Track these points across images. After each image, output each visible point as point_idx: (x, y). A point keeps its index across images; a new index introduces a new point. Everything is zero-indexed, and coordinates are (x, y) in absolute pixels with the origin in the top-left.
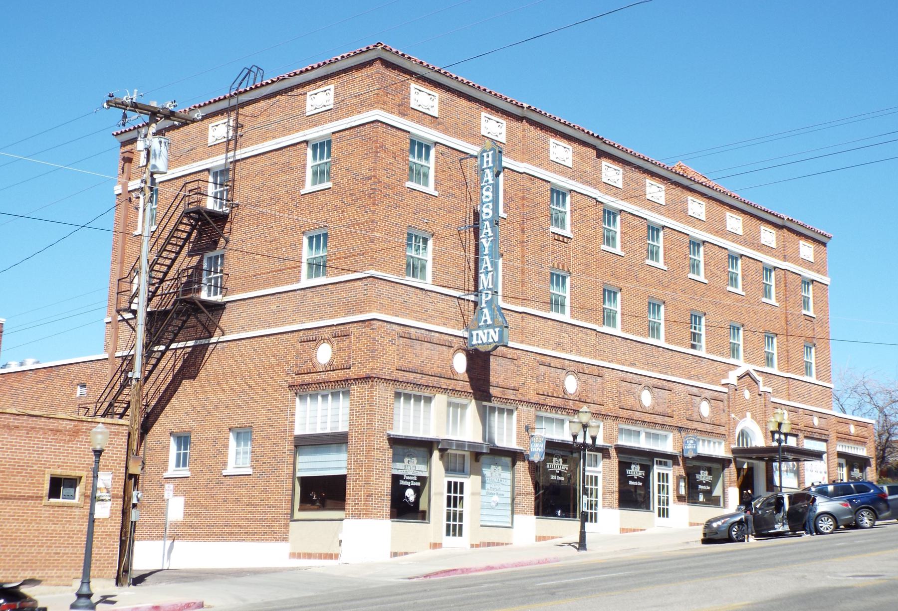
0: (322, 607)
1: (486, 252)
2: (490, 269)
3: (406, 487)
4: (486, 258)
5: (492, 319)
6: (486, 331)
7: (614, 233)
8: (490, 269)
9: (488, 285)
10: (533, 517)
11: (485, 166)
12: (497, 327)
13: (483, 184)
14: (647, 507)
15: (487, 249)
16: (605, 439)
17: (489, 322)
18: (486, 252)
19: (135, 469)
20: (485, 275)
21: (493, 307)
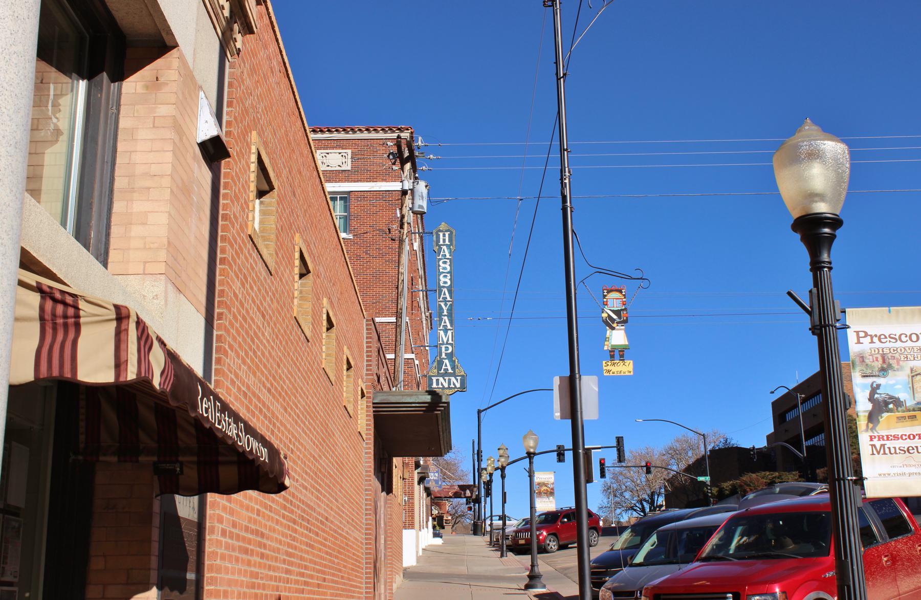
0: (277, 29)
1: (445, 313)
2: (449, 327)
3: (825, 267)
4: (446, 318)
5: (453, 368)
6: (447, 378)
7: (208, 579)
8: (449, 327)
9: (448, 340)
10: (881, 383)
11: (441, 242)
12: (459, 376)
13: (440, 257)
14: (413, 528)
15: (445, 311)
16: (208, 590)
17: (450, 371)
18: (445, 313)
19: (882, 475)
20: (444, 332)
21: (454, 359)
